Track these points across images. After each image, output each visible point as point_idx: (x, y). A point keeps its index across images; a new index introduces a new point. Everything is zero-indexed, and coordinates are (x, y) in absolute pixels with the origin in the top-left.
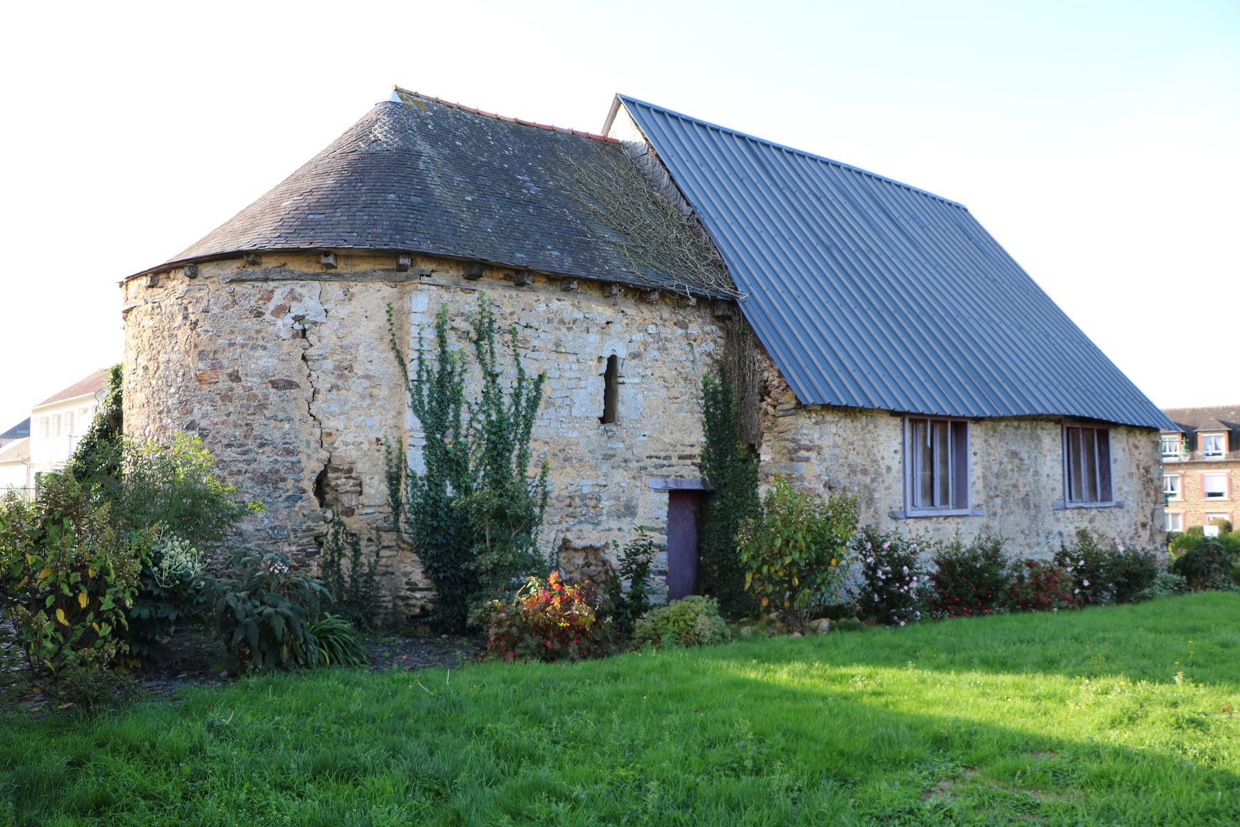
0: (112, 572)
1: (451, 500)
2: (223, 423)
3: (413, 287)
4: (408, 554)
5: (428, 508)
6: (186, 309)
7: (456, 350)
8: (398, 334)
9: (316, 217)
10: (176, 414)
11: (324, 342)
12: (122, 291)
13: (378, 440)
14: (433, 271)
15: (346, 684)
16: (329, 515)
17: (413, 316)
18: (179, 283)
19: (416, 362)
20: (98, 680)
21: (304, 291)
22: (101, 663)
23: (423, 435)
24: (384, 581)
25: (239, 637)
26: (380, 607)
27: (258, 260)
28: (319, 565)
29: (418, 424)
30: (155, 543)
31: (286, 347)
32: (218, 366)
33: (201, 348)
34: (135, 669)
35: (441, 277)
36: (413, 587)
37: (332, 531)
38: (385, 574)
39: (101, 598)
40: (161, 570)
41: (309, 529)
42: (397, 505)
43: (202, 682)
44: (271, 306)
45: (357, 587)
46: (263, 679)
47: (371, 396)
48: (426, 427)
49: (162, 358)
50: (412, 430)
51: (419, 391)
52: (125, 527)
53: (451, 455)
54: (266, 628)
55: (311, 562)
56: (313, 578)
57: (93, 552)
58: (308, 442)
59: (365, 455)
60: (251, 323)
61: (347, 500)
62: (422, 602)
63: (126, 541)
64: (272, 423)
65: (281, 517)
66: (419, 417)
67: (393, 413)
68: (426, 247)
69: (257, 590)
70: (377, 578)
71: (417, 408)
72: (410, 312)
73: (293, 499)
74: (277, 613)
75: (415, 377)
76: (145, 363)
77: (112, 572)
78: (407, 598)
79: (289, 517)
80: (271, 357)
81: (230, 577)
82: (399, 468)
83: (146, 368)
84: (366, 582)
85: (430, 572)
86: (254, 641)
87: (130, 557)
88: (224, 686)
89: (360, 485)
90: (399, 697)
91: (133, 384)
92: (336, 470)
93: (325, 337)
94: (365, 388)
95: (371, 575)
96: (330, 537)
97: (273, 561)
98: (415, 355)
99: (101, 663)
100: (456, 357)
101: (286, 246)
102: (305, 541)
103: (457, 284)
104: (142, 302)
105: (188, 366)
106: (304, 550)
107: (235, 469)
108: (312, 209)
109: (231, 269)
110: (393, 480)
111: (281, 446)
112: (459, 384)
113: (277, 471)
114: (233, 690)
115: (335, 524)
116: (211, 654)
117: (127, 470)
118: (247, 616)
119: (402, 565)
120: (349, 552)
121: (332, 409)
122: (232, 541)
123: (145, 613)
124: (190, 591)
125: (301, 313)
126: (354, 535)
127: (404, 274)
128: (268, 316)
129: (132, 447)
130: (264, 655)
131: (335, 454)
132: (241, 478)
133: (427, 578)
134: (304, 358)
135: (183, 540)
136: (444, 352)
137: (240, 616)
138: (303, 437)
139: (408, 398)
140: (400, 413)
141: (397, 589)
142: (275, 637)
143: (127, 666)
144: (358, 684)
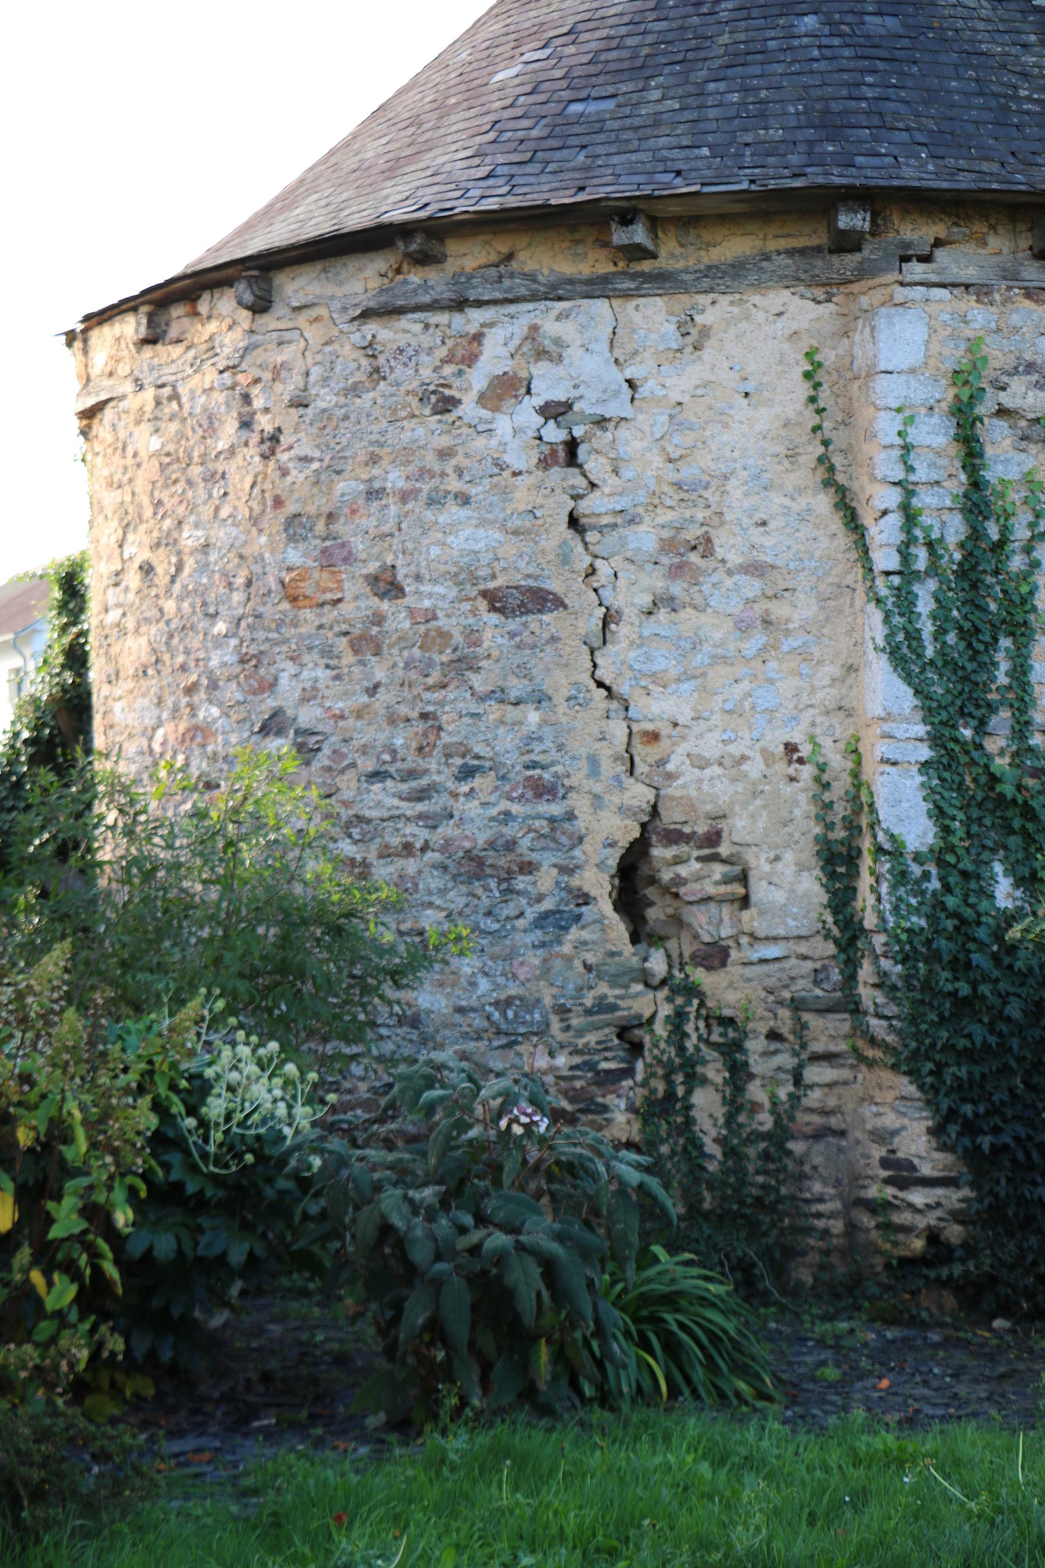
0: (80, 1134)
1: (1010, 918)
2: (359, 714)
3: (878, 295)
4: (887, 1076)
5: (942, 943)
6: (246, 398)
7: (1013, 473)
8: (839, 438)
9: (592, 107)
10: (232, 692)
11: (627, 473)
12: (69, 359)
13: (791, 748)
14: (938, 243)
15: (719, 1462)
16: (657, 964)
17: (882, 381)
18: (223, 324)
19: (895, 519)
20: (43, 1436)
21: (566, 330)
22: (50, 1387)
23: (921, 730)
24: (818, 1155)
25: (417, 1316)
26: (811, 1230)
27: (435, 248)
28: (631, 1109)
29: (905, 698)
30: (191, 1053)
31: (523, 494)
32: (339, 554)
33: (291, 508)
34: (139, 1401)
35: (960, 261)
36: (902, 1174)
37: (666, 1010)
38: (819, 1135)
39: (50, 1205)
40: (204, 1124)
41: (603, 1006)
42: (849, 935)
43: (319, 1443)
44: (478, 378)
45: (739, 1171)
46: (483, 1439)
47: (767, 622)
48: (930, 708)
49: (190, 538)
50: (888, 717)
51: (905, 600)
52: (111, 1009)
53: (1007, 789)
54: (490, 1291)
55: (610, 1100)
56: (618, 1146)
57: (26, 1078)
58: (593, 761)
59: (755, 794)
60: (426, 431)
61: (709, 923)
62: (931, 1219)
63: (115, 1049)
64: (493, 711)
65: (522, 973)
66: (908, 677)
67: (832, 670)
68: (917, 172)
69: (468, 1178)
70: (797, 1147)
71: (903, 653)
72: (872, 373)
73: (554, 923)
74: (520, 1247)
75: (893, 562)
76: (145, 555)
77: (80, 1134)
78: (887, 1206)
79: (545, 971)
80: (482, 523)
81: (389, 1144)
82: (852, 827)
83: (147, 570)
84: (766, 1156)
85: (953, 1129)
86: (460, 1330)
87: (127, 1091)
88: (380, 1455)
89: (743, 878)
90: (873, 1510)
91: (114, 615)
92: (674, 837)
93: (632, 460)
94: (749, 602)
95: (779, 1136)
96: (660, 1029)
97: (509, 1100)
98: (892, 498)
99: (50, 1387)
100: (1015, 496)
101: (512, 202)
102: (591, 1038)
103: (1011, 276)
104: (128, 387)
105: (259, 559)
106: (590, 1066)
107: (395, 841)
108: (579, 85)
109: (363, 279)
110: (838, 862)
111: (519, 774)
112: (1024, 576)
113: (511, 845)
114: (403, 1467)
115: (675, 991)
116: (341, 1360)
117: (108, 850)
118: (438, 1257)
119: (868, 1110)
120: (715, 1071)
121: (659, 664)
122: (393, 1040)
123: (165, 1245)
124: (283, 1184)
125: (560, 395)
126: (728, 1022)
127: (851, 260)
128: (469, 409)
129: (121, 788)
130: (486, 1368)
131: (672, 790)
132: (411, 865)
133: (942, 1148)
134: (574, 521)
135: (262, 1044)
136: (976, 485)
137: (420, 1255)
138: (580, 746)
139: (874, 626)
140: (851, 669)
141: (857, 1179)
142: (516, 1321)
143: (116, 1391)
144: (752, 1463)
